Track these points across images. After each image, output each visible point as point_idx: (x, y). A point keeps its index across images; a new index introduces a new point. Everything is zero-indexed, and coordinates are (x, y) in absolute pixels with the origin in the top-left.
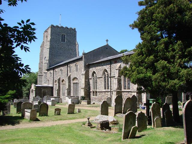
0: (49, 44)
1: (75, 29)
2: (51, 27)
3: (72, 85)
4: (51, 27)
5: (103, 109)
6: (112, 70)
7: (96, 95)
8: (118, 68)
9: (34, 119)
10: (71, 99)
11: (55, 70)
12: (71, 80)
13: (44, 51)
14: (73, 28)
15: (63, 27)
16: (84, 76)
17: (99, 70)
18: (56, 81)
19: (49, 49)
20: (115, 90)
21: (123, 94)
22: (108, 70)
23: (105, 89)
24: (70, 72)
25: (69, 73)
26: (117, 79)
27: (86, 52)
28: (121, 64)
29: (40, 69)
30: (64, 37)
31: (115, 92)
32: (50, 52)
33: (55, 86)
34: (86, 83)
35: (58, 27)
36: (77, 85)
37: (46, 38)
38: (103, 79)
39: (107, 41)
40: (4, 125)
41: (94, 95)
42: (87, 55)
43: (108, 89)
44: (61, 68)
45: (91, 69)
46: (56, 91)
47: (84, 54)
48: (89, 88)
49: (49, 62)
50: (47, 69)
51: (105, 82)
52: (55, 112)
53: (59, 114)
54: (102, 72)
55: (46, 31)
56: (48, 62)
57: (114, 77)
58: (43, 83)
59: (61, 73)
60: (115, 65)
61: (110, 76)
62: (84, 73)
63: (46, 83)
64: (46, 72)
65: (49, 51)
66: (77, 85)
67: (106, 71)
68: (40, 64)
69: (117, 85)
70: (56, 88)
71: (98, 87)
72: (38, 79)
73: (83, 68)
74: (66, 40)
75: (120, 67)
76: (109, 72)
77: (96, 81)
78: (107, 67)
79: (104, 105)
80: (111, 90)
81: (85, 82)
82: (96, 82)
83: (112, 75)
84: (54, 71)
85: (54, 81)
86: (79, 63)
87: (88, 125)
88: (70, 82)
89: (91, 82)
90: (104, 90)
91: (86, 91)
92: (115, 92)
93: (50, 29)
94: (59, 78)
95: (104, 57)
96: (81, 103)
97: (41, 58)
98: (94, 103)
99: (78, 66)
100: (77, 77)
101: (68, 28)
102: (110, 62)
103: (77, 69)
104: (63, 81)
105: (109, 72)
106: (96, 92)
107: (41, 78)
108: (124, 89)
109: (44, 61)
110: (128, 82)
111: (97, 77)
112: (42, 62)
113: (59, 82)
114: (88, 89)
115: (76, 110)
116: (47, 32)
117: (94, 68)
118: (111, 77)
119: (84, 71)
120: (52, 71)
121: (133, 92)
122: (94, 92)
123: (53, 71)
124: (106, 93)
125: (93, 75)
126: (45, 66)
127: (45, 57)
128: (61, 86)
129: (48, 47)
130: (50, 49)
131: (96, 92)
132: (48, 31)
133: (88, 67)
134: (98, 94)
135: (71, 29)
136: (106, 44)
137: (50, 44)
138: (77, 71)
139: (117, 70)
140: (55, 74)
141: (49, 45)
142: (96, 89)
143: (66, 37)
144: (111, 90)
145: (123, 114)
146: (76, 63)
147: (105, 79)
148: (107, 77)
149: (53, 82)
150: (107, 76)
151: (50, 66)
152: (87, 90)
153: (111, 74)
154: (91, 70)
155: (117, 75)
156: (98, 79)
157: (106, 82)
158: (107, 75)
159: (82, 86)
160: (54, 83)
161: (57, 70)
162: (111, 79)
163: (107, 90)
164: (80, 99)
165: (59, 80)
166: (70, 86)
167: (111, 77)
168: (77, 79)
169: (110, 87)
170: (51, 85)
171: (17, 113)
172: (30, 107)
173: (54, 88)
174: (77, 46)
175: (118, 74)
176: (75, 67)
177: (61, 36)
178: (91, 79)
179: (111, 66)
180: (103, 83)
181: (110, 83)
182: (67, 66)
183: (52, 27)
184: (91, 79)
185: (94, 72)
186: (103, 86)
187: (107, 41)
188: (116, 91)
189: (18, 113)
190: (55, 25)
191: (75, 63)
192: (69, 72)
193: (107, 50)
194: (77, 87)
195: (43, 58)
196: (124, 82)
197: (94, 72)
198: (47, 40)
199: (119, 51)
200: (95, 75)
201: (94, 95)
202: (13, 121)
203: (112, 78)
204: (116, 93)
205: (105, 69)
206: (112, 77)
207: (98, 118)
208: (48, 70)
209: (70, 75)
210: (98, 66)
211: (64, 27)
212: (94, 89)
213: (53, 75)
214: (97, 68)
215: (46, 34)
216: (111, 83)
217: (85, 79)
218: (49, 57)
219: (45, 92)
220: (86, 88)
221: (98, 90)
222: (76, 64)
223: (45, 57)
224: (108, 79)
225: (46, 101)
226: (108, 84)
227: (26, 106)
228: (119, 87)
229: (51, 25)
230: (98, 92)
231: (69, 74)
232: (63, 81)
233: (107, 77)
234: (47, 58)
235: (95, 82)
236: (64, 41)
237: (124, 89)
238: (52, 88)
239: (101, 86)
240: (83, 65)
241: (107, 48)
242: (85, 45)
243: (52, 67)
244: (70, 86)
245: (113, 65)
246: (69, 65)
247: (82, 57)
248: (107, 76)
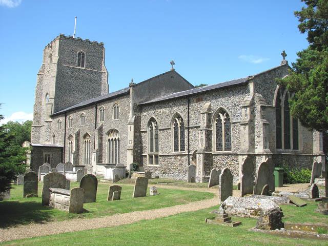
0: (54, 69)
1: (102, 44)
2: (59, 38)
3: (106, 143)
4: (60, 39)
5: (225, 184)
6: (192, 116)
7: (157, 163)
8: (248, 103)
9: (77, 210)
10: (113, 169)
11: (68, 117)
12: (104, 134)
13: (45, 82)
14: (99, 43)
15: (82, 40)
16: (133, 126)
17: (164, 116)
18: (71, 136)
19: (55, 79)
20: (202, 152)
21: (215, 159)
22: (184, 115)
23: (176, 149)
24: (102, 119)
25: (99, 121)
26: (204, 132)
27: (137, 82)
28: (210, 106)
29: (35, 114)
30: (83, 57)
31: (202, 155)
32: (57, 83)
33: (68, 146)
34: (136, 140)
35: (71, 38)
36: (116, 144)
37: (48, 60)
38: (172, 132)
39: (172, 63)
40: (23, 224)
41: (151, 163)
42: (138, 88)
43: (183, 149)
44: (83, 112)
45: (145, 114)
46: (72, 155)
47: (134, 86)
48: (141, 148)
49: (55, 102)
50: (50, 114)
51: (176, 137)
52: (111, 193)
53: (119, 199)
54: (168, 120)
55: (49, 46)
56: (52, 101)
57: (199, 127)
58: (43, 139)
59: (80, 122)
60: (197, 105)
61: (187, 126)
62: (133, 121)
63: (49, 141)
64: (50, 120)
65: (56, 81)
66: (116, 144)
67: (179, 117)
68: (35, 105)
69: (204, 142)
70: (70, 148)
71: (160, 146)
72: (32, 133)
73: (131, 111)
74: (85, 63)
75: (209, 109)
76: (185, 119)
77: (157, 135)
78: (181, 110)
79: (225, 177)
80: (189, 152)
81: (135, 137)
82: (157, 138)
83: (190, 123)
84: (67, 119)
85: (67, 137)
86: (120, 102)
87: (225, 220)
88: (101, 138)
89: (146, 138)
90: (175, 153)
91: (135, 154)
92: (202, 155)
93: (57, 42)
94: (77, 130)
95: (167, 92)
96: (130, 177)
97: (39, 96)
98: (157, 177)
99: (119, 108)
100: (117, 129)
101: (90, 42)
102: (188, 99)
103: (118, 114)
104: (86, 136)
105: (185, 119)
106: (157, 156)
107: (39, 132)
108: (218, 149)
109: (44, 101)
110: (225, 136)
111: (160, 128)
112: (40, 103)
113: (78, 138)
114: (139, 151)
115: (150, 192)
116: (51, 47)
117: (151, 112)
118: (188, 128)
119: (132, 117)
120: (62, 119)
121: (240, 155)
122: (151, 157)
123: (64, 118)
124: (179, 157)
125: (150, 123)
126: (47, 108)
127: (47, 94)
128: (82, 146)
129: (55, 74)
130: (56, 78)
131: (157, 156)
132: (53, 45)
133: (140, 108)
134: (160, 159)
135: (96, 43)
136: (168, 69)
137: (58, 69)
138: (103, 120)
139: (203, 114)
140: (68, 125)
141: (56, 70)
142: (157, 150)
143: (85, 57)
144: (189, 152)
145: (263, 194)
146: (115, 102)
147: (176, 133)
148: (181, 131)
149: (64, 139)
150: (154, 128)
151: (56, 110)
152: (137, 153)
153: (188, 123)
154: (146, 115)
155: (203, 124)
156: (160, 132)
157: (177, 136)
158: (155, 127)
159: (129, 145)
160: (67, 140)
161: (72, 116)
162: (188, 130)
163: (179, 152)
164: (128, 168)
165: (78, 134)
166: (101, 145)
167: (188, 128)
168: (117, 131)
169: (186, 147)
170: (58, 145)
171: (24, 196)
172: (60, 184)
173: (67, 149)
174: (104, 77)
175: (205, 121)
176: (113, 110)
177: (77, 55)
178: (145, 132)
179: (189, 106)
180: (172, 139)
181: (186, 139)
182: (95, 109)
183: (62, 37)
184: (145, 132)
185: (152, 119)
186: (172, 144)
187: (172, 63)
188: (203, 153)
189: (28, 197)
190: (67, 35)
191: (112, 103)
192: (99, 119)
193: (171, 79)
194: (116, 147)
195: (41, 95)
196: (217, 137)
197: (152, 119)
198: (51, 62)
199: (194, 86)
200: (153, 125)
201: (151, 163)
202: (36, 213)
203: (191, 130)
204: (204, 157)
205: (177, 114)
206: (191, 128)
207: (231, 205)
208: (53, 117)
209: (102, 125)
210: (161, 108)
211: (84, 39)
212: (152, 150)
213: (64, 126)
214: (159, 111)
215: (48, 51)
216: (189, 140)
217: (135, 132)
218: (56, 93)
219: (49, 158)
220: (136, 149)
221: (160, 153)
222: (114, 105)
223: (47, 94)
224: (183, 133)
225: (65, 173)
226: (183, 141)
227: (52, 181)
228: (209, 146)
229: (59, 35)
230: (160, 156)
231: (100, 123)
232: (86, 136)
233: (181, 131)
234: (52, 95)
235: (155, 139)
236: (83, 66)
237: (218, 149)
238: (62, 150)
239: (167, 144)
240: (131, 106)
241: (172, 77)
242: (119, 75)
243: (61, 111)
244: (101, 145)
245: (195, 106)
246: (98, 107)
247: (129, 92)
248: (154, 128)
